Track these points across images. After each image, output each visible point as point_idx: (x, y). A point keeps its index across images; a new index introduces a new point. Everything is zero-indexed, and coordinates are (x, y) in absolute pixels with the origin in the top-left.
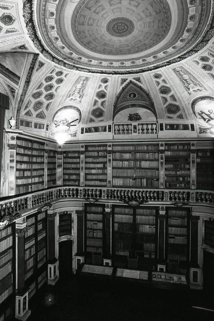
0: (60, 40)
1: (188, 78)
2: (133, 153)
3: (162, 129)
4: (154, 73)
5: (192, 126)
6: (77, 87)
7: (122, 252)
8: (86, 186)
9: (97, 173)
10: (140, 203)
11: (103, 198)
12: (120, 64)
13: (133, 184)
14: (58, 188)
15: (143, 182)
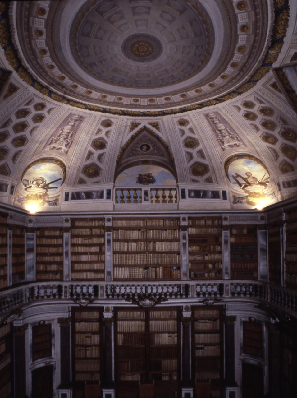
0: (48, 54)
1: (223, 128)
2: (144, 230)
3: (184, 197)
4: (178, 119)
5: (224, 193)
6: (64, 130)
7: (131, 375)
8: (72, 280)
9: (90, 260)
10: (157, 303)
11: (100, 298)
12: (132, 100)
13: (144, 275)
14: (31, 285)
15: (158, 272)
